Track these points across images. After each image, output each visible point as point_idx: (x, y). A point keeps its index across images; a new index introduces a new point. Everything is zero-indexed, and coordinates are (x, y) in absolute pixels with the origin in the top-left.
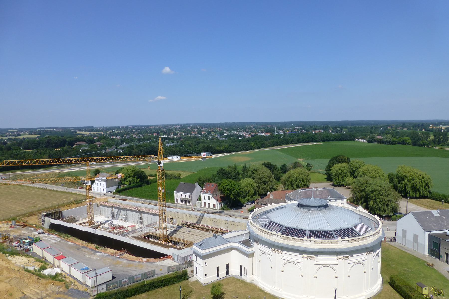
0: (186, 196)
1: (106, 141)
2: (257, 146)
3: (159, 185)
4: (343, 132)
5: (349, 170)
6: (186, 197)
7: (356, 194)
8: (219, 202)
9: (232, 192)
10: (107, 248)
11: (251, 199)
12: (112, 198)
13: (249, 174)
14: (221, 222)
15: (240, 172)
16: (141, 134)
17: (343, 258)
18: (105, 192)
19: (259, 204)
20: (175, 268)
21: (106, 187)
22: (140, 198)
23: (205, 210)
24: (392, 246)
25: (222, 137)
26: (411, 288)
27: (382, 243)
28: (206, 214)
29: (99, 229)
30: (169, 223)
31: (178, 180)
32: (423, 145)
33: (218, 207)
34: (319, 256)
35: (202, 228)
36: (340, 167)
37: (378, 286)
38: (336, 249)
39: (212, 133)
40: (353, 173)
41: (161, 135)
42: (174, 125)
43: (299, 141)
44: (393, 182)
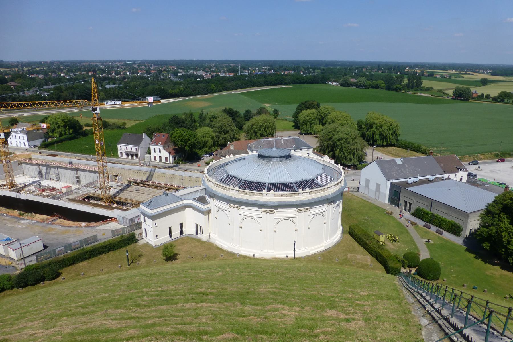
0: (133, 149)
1: (24, 81)
2: (218, 89)
3: (96, 137)
4: (315, 74)
5: (317, 116)
6: (132, 150)
7: (323, 143)
8: (171, 155)
9: (186, 143)
10: (34, 214)
11: (209, 151)
12: (37, 153)
13: (207, 121)
14: (174, 177)
15: (197, 118)
16: (72, 72)
17: (303, 210)
18: (27, 146)
19: (218, 156)
20: (120, 231)
21: (28, 141)
22: (74, 153)
23: (156, 164)
24: (355, 196)
25: (176, 78)
26: (369, 236)
27: (344, 194)
28: (158, 170)
29: (23, 192)
30: (112, 182)
31: (123, 130)
32: (396, 90)
33: (171, 160)
34: (279, 210)
35: (153, 186)
36: (308, 114)
37: (337, 236)
38: (296, 201)
39: (164, 72)
40: (322, 120)
41: (99, 74)
42: (115, 62)
43: (267, 83)
44: (362, 129)
